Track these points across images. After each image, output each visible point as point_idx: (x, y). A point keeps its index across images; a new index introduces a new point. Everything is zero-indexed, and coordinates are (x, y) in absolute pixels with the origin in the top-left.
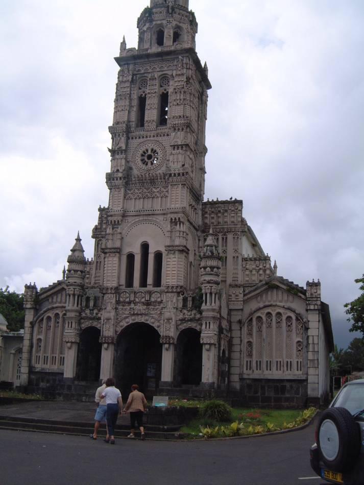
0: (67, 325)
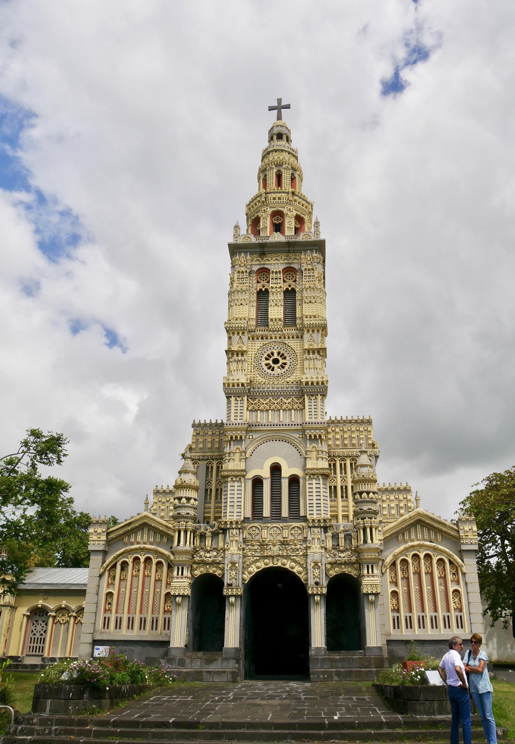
0: (175, 573)
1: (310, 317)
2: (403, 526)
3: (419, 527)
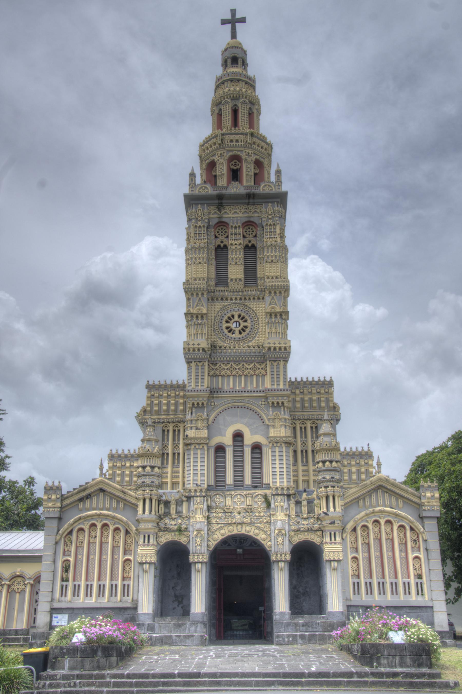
1: (272, 278)
2: (364, 492)
3: (380, 492)
